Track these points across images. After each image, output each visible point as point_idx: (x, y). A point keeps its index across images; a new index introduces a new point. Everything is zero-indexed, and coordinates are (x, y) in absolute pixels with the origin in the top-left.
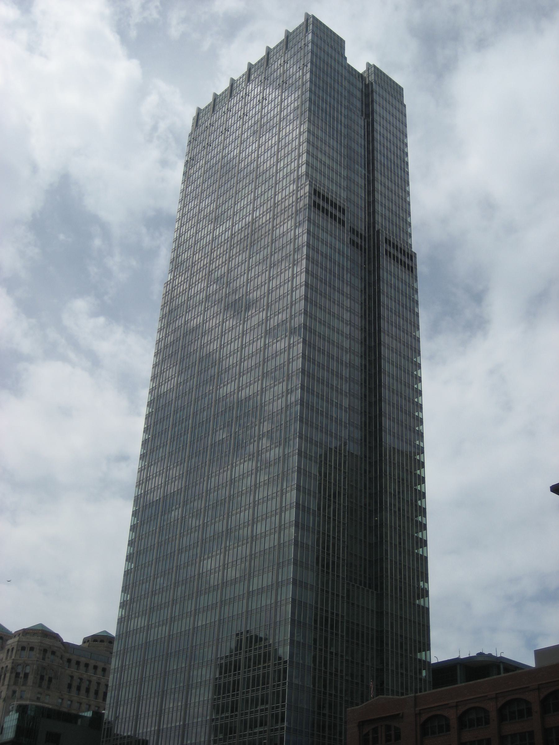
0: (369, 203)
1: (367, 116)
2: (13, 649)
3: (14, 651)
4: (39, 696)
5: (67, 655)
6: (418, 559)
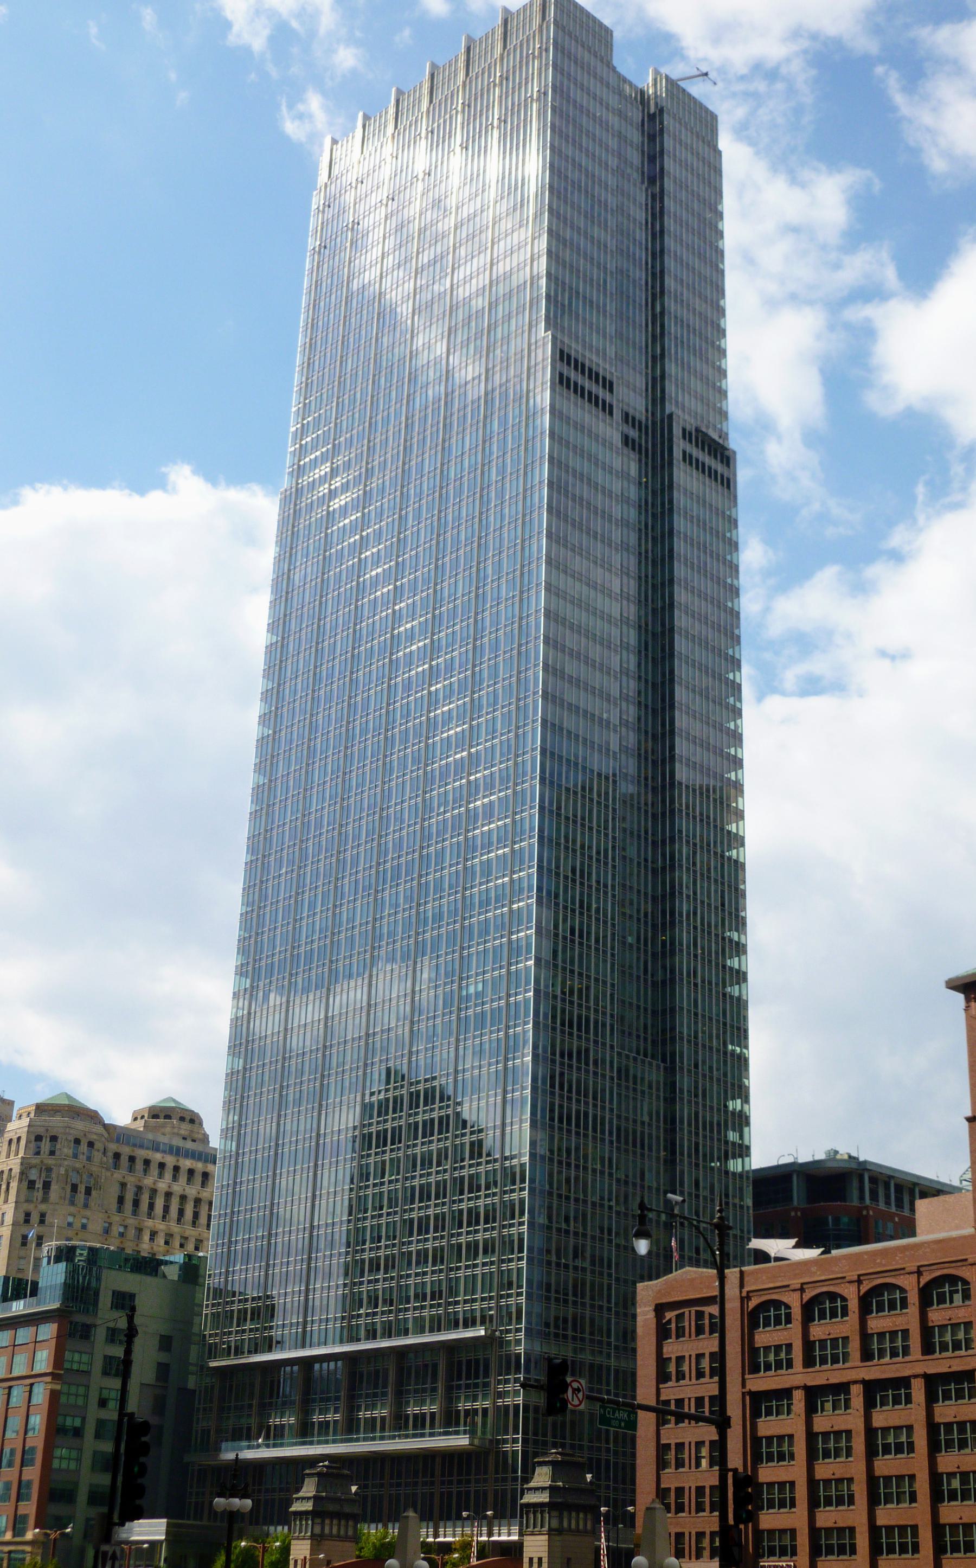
0: (654, 379)
1: (652, 181)
2: (19, 1139)
3: (23, 1142)
4: (70, 1219)
5: (113, 1147)
6: (732, 1003)
